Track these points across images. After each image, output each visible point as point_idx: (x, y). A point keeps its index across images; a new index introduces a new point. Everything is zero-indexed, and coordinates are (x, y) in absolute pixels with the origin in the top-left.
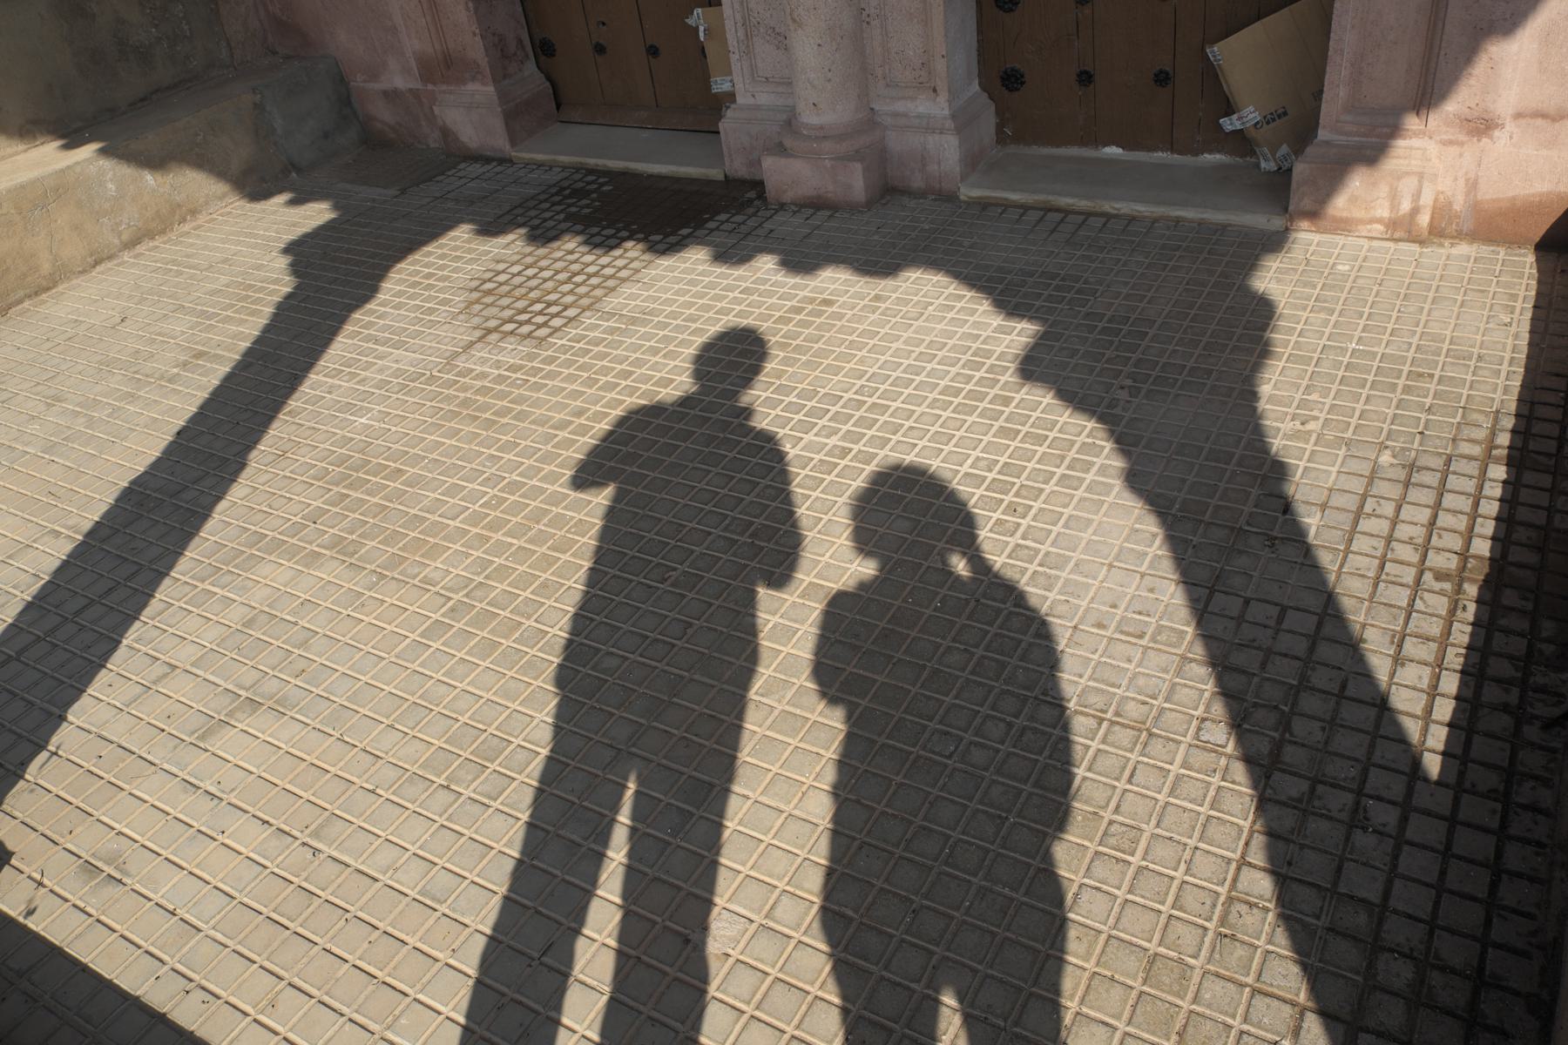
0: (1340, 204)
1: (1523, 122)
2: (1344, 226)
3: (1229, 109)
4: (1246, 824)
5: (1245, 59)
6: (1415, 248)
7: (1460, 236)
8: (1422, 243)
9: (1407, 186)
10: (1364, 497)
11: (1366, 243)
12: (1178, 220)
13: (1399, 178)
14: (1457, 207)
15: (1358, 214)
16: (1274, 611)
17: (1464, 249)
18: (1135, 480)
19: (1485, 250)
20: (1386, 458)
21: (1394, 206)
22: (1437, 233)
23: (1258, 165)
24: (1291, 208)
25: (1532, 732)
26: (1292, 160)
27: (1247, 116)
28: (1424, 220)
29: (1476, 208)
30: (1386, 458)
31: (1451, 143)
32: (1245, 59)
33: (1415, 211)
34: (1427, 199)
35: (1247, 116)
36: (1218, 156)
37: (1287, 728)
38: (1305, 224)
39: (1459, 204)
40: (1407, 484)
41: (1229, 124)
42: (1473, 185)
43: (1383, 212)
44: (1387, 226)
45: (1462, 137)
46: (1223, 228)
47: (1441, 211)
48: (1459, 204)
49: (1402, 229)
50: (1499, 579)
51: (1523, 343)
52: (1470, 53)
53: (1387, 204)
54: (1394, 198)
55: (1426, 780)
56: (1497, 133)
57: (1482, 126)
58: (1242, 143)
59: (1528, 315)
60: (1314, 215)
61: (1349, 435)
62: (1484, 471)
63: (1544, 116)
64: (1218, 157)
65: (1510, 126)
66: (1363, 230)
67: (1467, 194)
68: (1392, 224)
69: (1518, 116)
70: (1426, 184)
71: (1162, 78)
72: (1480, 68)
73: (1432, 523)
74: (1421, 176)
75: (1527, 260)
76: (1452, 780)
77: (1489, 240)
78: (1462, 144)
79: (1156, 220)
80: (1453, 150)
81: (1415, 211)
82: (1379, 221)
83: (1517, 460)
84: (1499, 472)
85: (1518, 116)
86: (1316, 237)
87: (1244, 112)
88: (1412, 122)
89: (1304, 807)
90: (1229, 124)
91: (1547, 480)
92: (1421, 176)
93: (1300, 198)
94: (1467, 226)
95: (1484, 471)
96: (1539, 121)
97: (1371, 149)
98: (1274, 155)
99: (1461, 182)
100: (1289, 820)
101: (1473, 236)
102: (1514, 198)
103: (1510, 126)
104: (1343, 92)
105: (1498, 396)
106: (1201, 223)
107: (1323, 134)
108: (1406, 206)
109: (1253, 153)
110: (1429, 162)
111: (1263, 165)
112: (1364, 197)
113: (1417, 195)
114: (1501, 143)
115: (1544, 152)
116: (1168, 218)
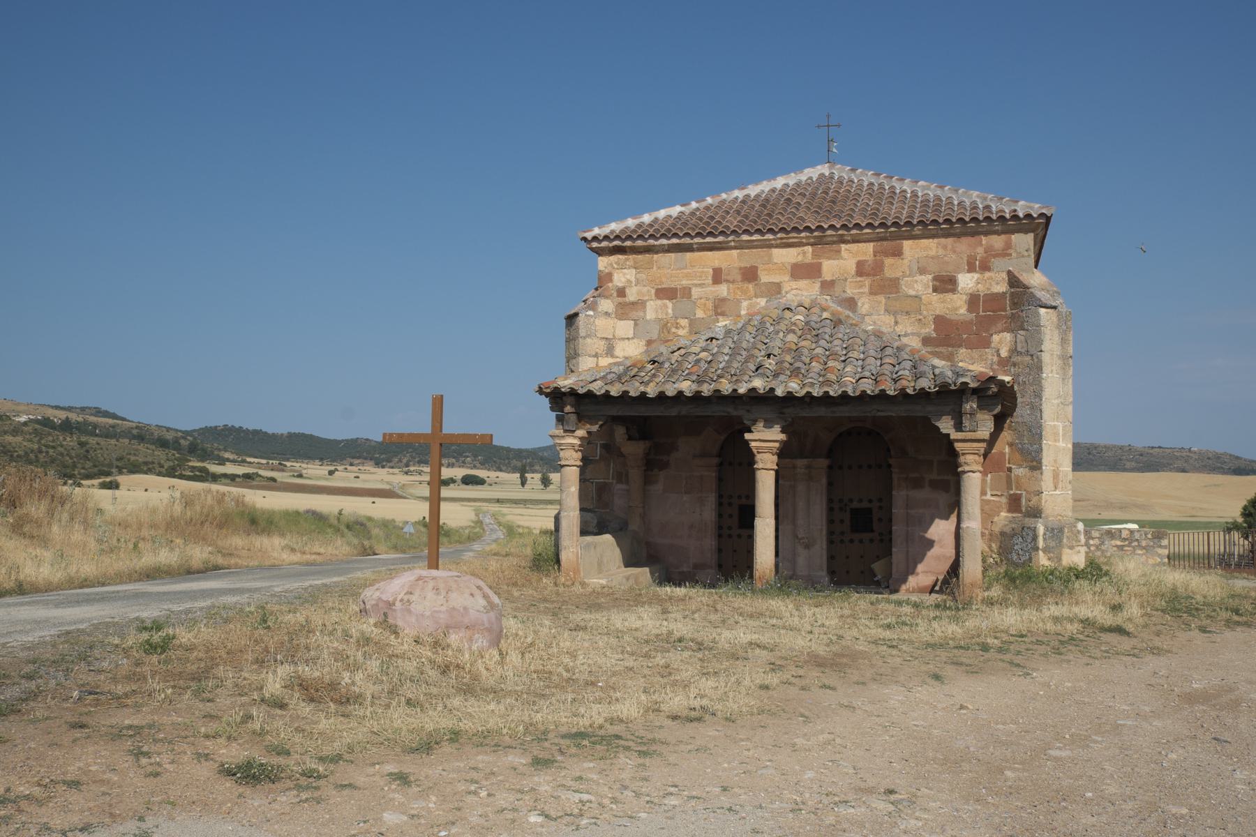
5: (877, 567)
32: (877, 567)
49: (908, 591)
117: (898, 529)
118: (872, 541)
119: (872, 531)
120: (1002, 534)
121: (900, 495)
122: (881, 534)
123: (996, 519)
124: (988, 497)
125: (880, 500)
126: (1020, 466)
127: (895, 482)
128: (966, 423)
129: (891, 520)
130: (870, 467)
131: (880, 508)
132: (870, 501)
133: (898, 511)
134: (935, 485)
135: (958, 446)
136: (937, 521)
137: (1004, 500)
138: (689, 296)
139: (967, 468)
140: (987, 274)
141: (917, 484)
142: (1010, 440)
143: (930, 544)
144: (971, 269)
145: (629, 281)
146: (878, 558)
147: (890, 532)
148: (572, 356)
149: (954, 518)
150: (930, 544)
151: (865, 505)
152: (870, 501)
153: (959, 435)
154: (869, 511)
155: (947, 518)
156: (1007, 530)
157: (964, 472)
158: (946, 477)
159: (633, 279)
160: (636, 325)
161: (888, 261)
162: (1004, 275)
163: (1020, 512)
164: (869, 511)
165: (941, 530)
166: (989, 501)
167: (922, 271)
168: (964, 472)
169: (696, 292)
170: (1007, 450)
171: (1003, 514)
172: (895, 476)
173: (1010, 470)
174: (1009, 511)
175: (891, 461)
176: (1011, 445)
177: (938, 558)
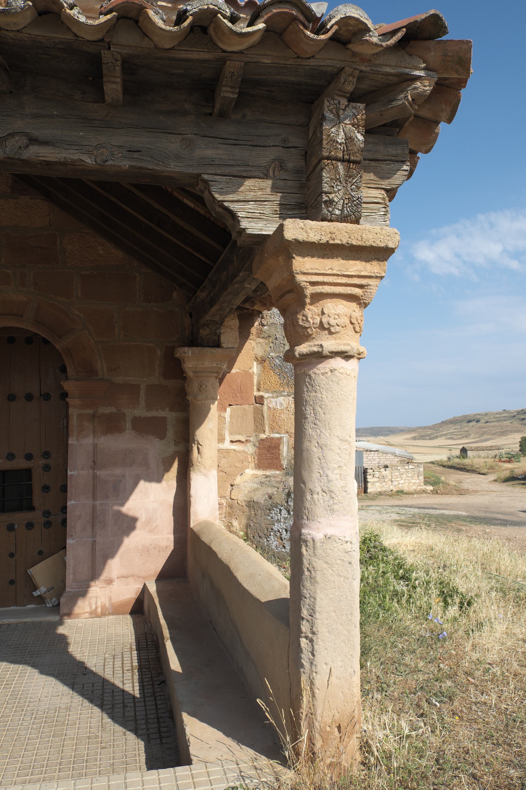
0: (77, 610)
1: (119, 579)
2: (78, 616)
3: (35, 588)
4: (101, 714)
5: (40, 572)
6: (98, 619)
7: (109, 614)
8: (100, 617)
9: (93, 601)
10: (104, 663)
11: (85, 620)
12: (25, 623)
13: (91, 599)
14: (107, 605)
15: (81, 611)
16: (91, 685)
17: (111, 617)
18: (41, 672)
19: (117, 616)
20: (107, 656)
21: (91, 608)
22: (103, 614)
23: (46, 606)
24: (61, 613)
25: (156, 686)
26: (60, 599)
27: (42, 590)
28: (99, 610)
29: (112, 605)
30: (107, 656)
31: (103, 587)
32: (40, 572)
33: (97, 608)
34: (99, 604)
35: (42, 590)
36: (32, 606)
37: (103, 699)
38: (66, 617)
39: (107, 605)
40: (114, 659)
41: (36, 594)
42: (110, 599)
43: (88, 610)
44: (89, 614)
45: (105, 586)
46: (41, 622)
47: (103, 607)
48: (107, 605)
49: (94, 614)
50: (141, 669)
51: (133, 630)
52: (104, 563)
53: (88, 607)
54: (90, 605)
55: (137, 698)
56: (114, 583)
57: (110, 582)
58: (41, 599)
59: (132, 626)
60: (69, 614)
61: (96, 653)
62: (131, 653)
63: (124, 577)
64: (32, 606)
65: (116, 581)
66: (83, 616)
67: (109, 601)
68: (91, 613)
69: (118, 578)
70: (98, 599)
71: (12, 582)
72: (107, 567)
73: (123, 663)
74: (96, 597)
75: (129, 616)
76: (142, 696)
77: (215, 44)
78: (105, 587)
79: (17, 624)
80: (103, 589)
81: (97, 608)
82: (87, 613)
83: (138, 649)
84: (135, 653)
85: (118, 578)
86: (70, 621)
87: (41, 589)
88: (92, 584)
89: (113, 708)
90: (36, 594)
91: (146, 651)
92: (96, 597)
93: (64, 610)
94: (111, 611)
95: (131, 653)
96: (123, 579)
97: (83, 593)
98: (51, 601)
99: (107, 598)
100: (110, 711)
101: (113, 614)
102: (121, 601)
103: (116, 581)
104: (71, 577)
105: (130, 640)
106: (33, 622)
107: (67, 589)
108: (94, 607)
109: (45, 603)
110: (99, 594)
111: (48, 605)
112: (83, 607)
113: (96, 603)
114: (116, 586)
115: (126, 587)
116: (21, 623)
117: (77, 505)
118: (30, 526)
119: (31, 508)
120: (251, 504)
121: (81, 446)
122: (47, 513)
123: (238, 480)
124: (227, 445)
125: (46, 455)
126: (279, 394)
127: (74, 421)
128: (333, 184)
129: (64, 489)
130: (29, 397)
131: (47, 468)
132: (29, 457)
133: (78, 473)
134: (143, 427)
135: (305, 266)
136: (142, 485)
137: (250, 449)
139: (329, 344)
141: (112, 425)
142: (259, 352)
143: (129, 524)
146: (42, 555)
147: (64, 509)
148: (95, 446)
149: (171, 479)
150: (129, 524)
151: (20, 463)
152: (29, 457)
153: (296, 229)
154: (28, 472)
155: (159, 480)
156: (260, 497)
157: (319, 356)
158: (161, 414)
163: (279, 467)
164: (28, 472)
165: (150, 501)
166: (228, 451)
168: (319, 356)
170: (255, 368)
171: (250, 472)
172: (74, 413)
173: (260, 400)
174: (259, 466)
175: (68, 386)
176: (261, 361)
177: (146, 551)
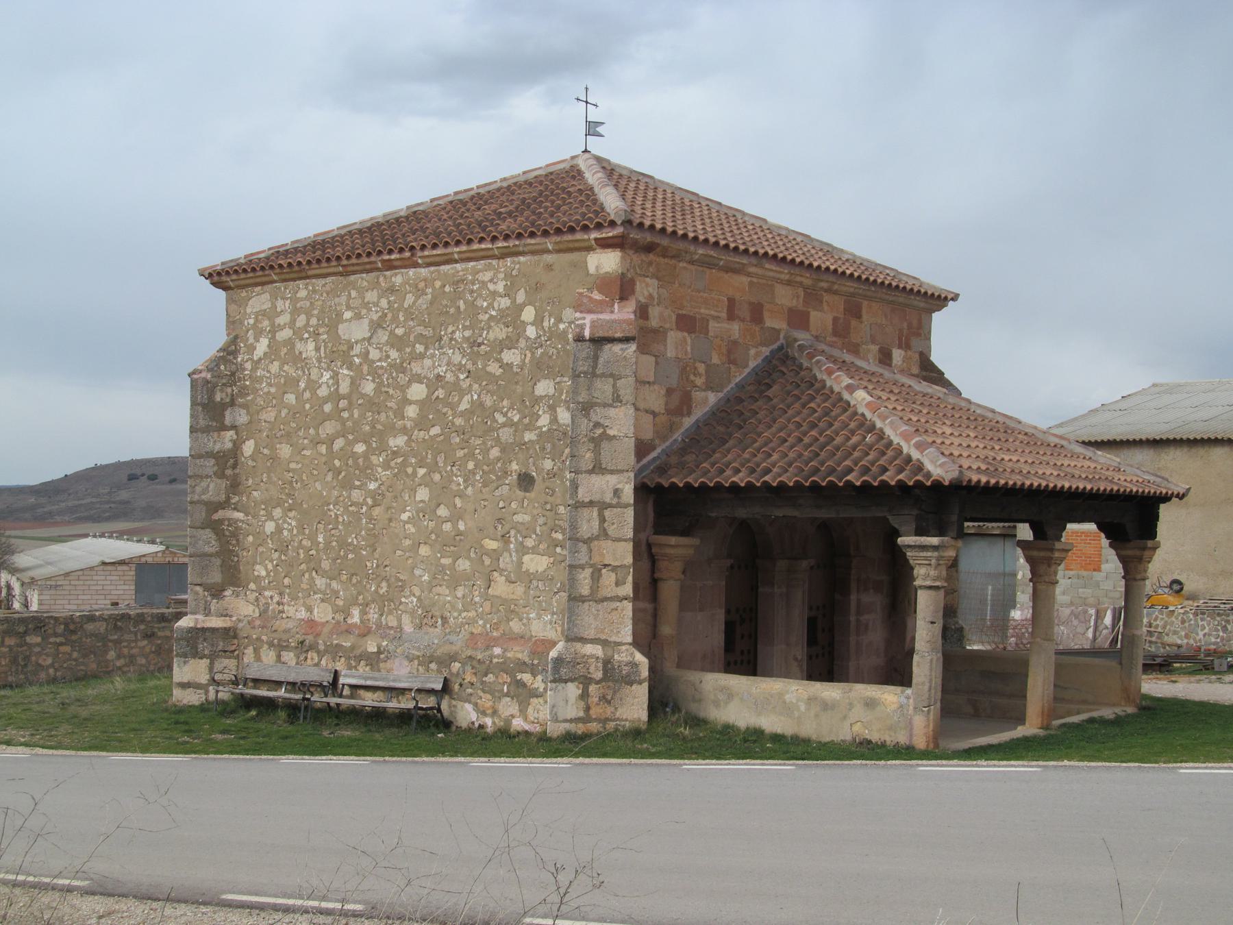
138: (706, 331)
140: (909, 353)
144: (900, 347)
145: (651, 296)
159: (656, 296)
160: (657, 363)
161: (854, 323)
162: (917, 356)
167: (873, 342)
169: (713, 325)
